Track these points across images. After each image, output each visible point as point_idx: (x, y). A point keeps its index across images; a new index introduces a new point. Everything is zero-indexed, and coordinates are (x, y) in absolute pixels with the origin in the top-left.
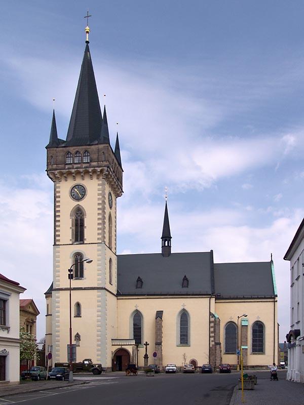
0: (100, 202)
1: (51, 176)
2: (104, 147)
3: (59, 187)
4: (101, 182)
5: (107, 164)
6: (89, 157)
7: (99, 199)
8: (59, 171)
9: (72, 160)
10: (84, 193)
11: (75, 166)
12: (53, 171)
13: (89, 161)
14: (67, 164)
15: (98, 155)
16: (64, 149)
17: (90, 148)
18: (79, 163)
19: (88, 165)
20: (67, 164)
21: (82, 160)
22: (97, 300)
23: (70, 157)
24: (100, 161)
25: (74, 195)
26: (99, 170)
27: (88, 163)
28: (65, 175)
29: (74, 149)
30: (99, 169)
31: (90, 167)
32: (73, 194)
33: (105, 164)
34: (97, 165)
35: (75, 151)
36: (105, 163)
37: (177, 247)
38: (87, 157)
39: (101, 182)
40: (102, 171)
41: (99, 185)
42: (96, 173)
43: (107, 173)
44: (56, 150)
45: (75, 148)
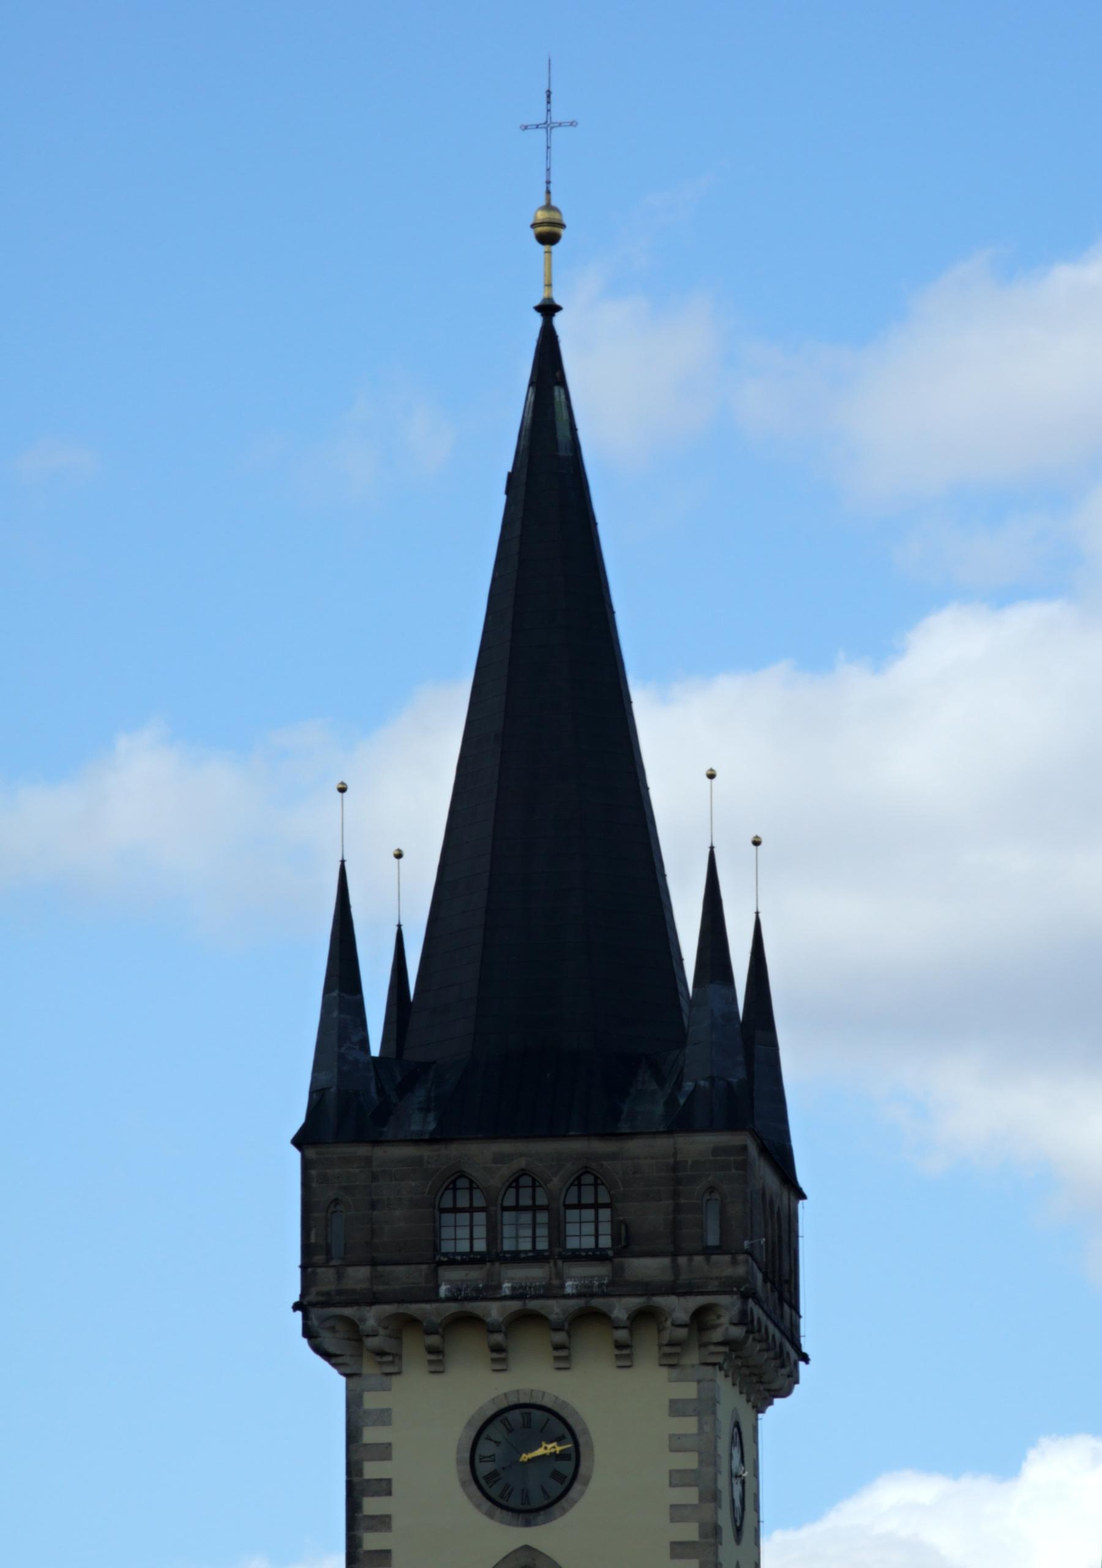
0: (690, 1532)
1: (329, 1342)
2: (716, 1151)
3: (384, 1417)
4: (688, 1391)
5: (741, 1270)
6: (605, 1214)
7: (677, 1513)
8: (390, 1309)
9: (480, 1232)
10: (566, 1468)
11: (511, 1277)
12: (348, 1311)
13: (605, 1242)
14: (454, 1261)
15: (677, 1209)
16: (425, 1152)
17: (614, 1156)
18: (536, 1257)
19: (598, 1272)
20: (454, 1261)
21: (557, 1233)
22: (673, 1403)
23: (471, 1210)
24: (691, 1254)
25: (493, 1477)
26: (683, 1316)
27: (596, 1256)
28: (371, 1342)
29: (499, 1159)
30: (680, 1308)
31: (618, 1286)
32: (484, 1469)
33: (729, 1271)
34: (668, 1277)
35: (506, 1171)
36: (723, 1267)
37: (567, 1238)
38: (589, 1214)
39: (688, 1391)
40: (700, 1319)
41: (677, 1408)
42: (660, 1330)
43: (738, 1332)
44: (368, 1160)
45: (505, 1147)
